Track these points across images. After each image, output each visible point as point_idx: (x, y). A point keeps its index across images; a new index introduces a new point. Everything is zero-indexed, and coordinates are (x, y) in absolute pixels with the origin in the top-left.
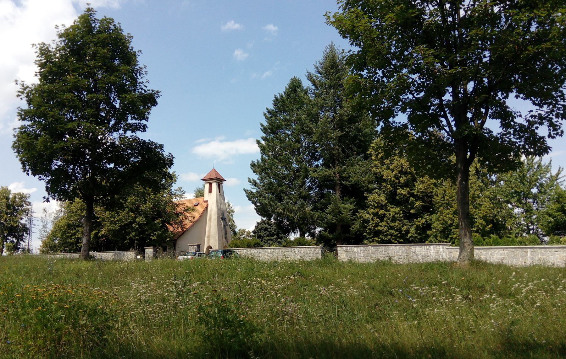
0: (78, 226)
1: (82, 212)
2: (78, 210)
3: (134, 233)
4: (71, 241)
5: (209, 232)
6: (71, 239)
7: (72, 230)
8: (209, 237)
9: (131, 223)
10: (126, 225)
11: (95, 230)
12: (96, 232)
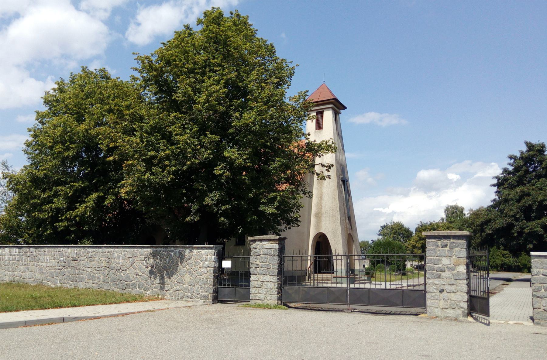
0: (59, 183)
1: (68, 149)
2: (55, 143)
3: (216, 195)
4: (41, 216)
5: (320, 206)
6: (41, 211)
7: (44, 191)
8: (318, 215)
9: (210, 165)
10: (193, 170)
11: (97, 191)
12: (99, 197)
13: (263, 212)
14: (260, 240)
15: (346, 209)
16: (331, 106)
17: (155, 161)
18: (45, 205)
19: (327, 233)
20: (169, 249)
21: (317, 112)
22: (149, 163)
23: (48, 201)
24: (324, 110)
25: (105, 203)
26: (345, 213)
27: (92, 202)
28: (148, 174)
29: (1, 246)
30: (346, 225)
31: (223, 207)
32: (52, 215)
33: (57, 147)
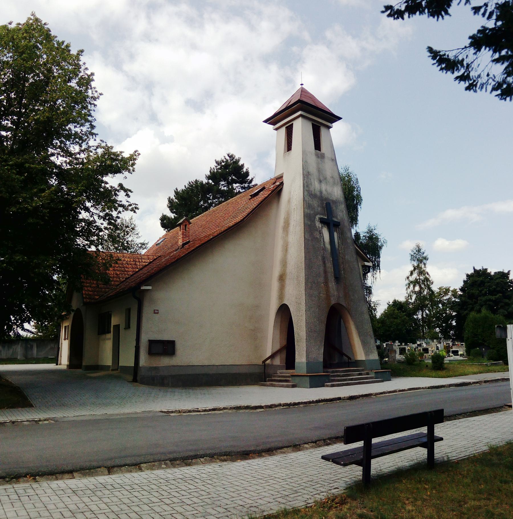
5: (284, 263)
8: (282, 278)
26: (325, 272)
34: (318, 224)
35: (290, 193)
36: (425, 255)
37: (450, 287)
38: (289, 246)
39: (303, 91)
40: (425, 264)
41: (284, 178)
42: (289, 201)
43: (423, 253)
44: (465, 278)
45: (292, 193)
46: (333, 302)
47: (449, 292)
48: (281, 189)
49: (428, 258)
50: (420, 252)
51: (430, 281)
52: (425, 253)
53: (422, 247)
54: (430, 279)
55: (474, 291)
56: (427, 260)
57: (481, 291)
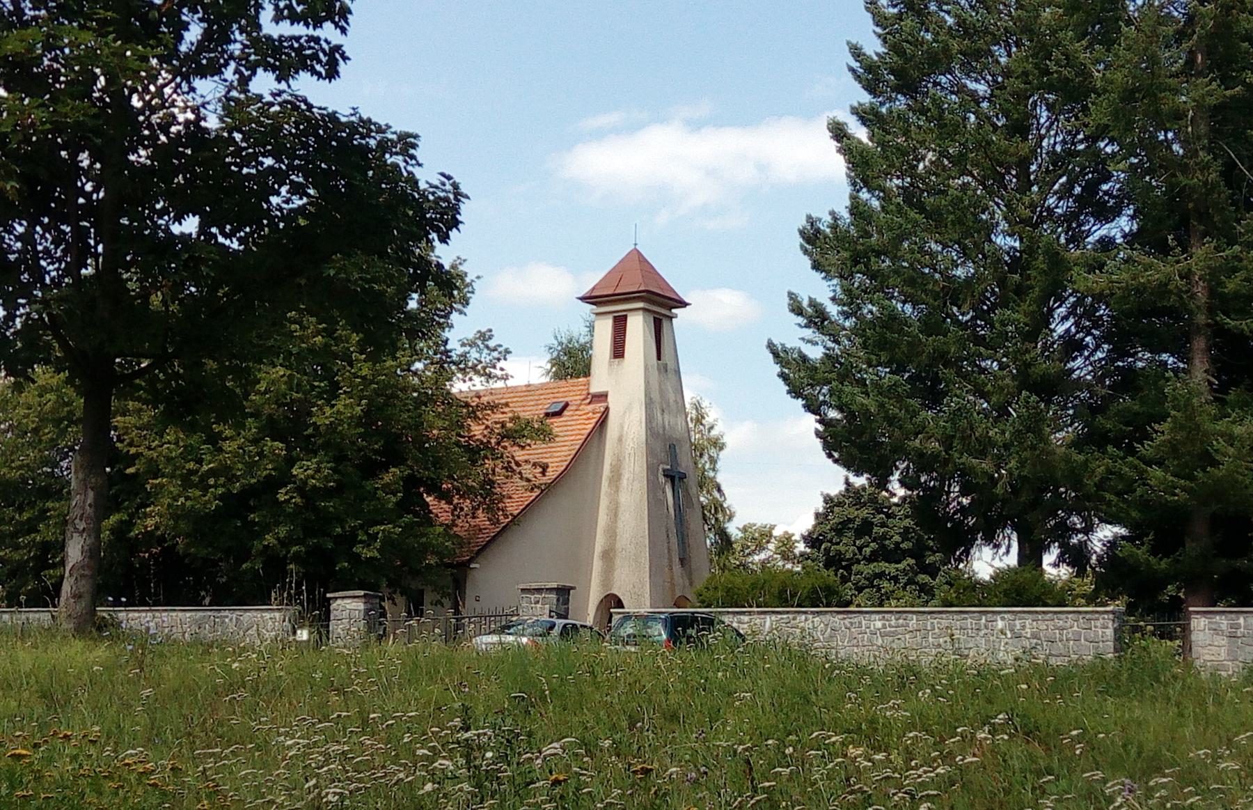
2: (43, 420)
5: (612, 533)
7: (20, 510)
8: (608, 555)
9: (271, 485)
10: (248, 492)
13: (358, 555)
14: (343, 598)
15: (674, 540)
16: (641, 305)
17: (195, 479)
18: (23, 536)
19: (624, 595)
20: (223, 614)
21: (615, 317)
22: (186, 481)
23: (31, 528)
24: (629, 314)
25: (132, 534)
26: (669, 550)
27: (108, 532)
28: (182, 499)
29: (1243, 313)
30: (672, 579)
31: (295, 549)
32: (35, 555)
33: (46, 431)
34: (662, 479)
35: (622, 427)
36: (714, 433)
37: (773, 527)
38: (621, 509)
39: (637, 259)
40: (713, 461)
41: (609, 398)
42: (620, 439)
43: (712, 428)
44: (820, 506)
45: (625, 429)
46: (678, 594)
47: (768, 542)
48: (607, 416)
49: (723, 444)
50: (702, 424)
51: (723, 510)
52: (716, 427)
53: (707, 410)
54: (725, 505)
55: (841, 548)
56: (721, 449)
57: (860, 549)
